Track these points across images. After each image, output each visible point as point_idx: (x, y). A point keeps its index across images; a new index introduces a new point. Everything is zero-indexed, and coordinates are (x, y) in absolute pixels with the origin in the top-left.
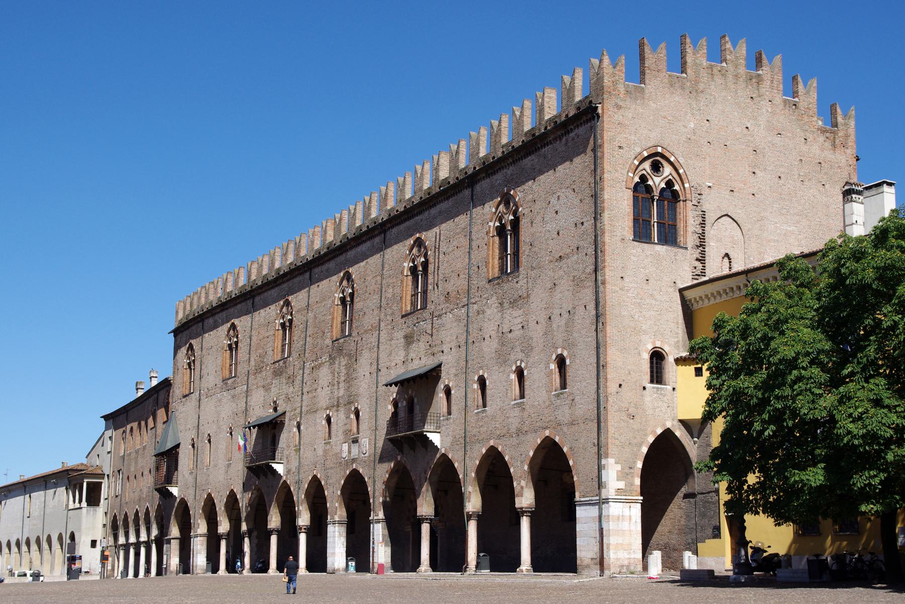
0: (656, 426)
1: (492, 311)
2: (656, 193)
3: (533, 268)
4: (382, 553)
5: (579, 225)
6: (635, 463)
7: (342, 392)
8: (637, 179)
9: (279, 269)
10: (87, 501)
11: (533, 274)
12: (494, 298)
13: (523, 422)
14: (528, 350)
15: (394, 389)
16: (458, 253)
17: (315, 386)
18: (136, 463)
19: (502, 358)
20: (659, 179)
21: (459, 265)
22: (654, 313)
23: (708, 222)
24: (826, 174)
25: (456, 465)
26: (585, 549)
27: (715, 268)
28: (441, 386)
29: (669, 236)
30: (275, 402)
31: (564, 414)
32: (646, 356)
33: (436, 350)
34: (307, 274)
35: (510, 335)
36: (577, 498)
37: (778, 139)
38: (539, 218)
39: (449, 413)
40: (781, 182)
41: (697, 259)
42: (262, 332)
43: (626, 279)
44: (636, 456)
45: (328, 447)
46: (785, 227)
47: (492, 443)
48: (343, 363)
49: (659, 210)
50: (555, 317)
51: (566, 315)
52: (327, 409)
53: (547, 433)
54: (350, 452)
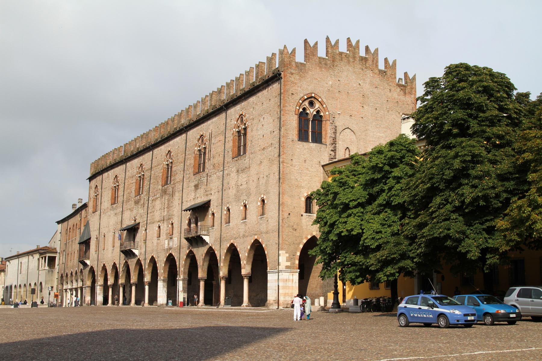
0: (308, 235)
1: (234, 175)
2: (311, 117)
3: (252, 153)
4: (181, 296)
5: (272, 133)
6: (296, 253)
7: (166, 213)
8: (301, 110)
9: (138, 148)
10: (48, 265)
11: (251, 156)
12: (235, 168)
13: (245, 232)
14: (249, 195)
15: (189, 213)
16: (219, 144)
17: (154, 210)
18: (72, 247)
19: (237, 198)
20: (313, 110)
21: (220, 150)
22: (308, 178)
23: (339, 131)
24: (400, 107)
25: (216, 252)
26: (271, 295)
27: (341, 154)
28: (210, 212)
29: (318, 139)
30: (135, 217)
31: (263, 228)
32: (303, 199)
33: (208, 193)
34: (151, 152)
35: (241, 187)
36: (268, 271)
37: (375, 90)
38: (255, 128)
39: (213, 226)
40: (377, 111)
41: (332, 150)
42: (130, 181)
43: (294, 161)
44: (296, 249)
45: (159, 241)
46: (378, 134)
47: (232, 242)
48: (166, 198)
49: (311, 127)
50: (261, 179)
51: (265, 178)
52: (159, 222)
53: (256, 237)
54: (169, 244)
